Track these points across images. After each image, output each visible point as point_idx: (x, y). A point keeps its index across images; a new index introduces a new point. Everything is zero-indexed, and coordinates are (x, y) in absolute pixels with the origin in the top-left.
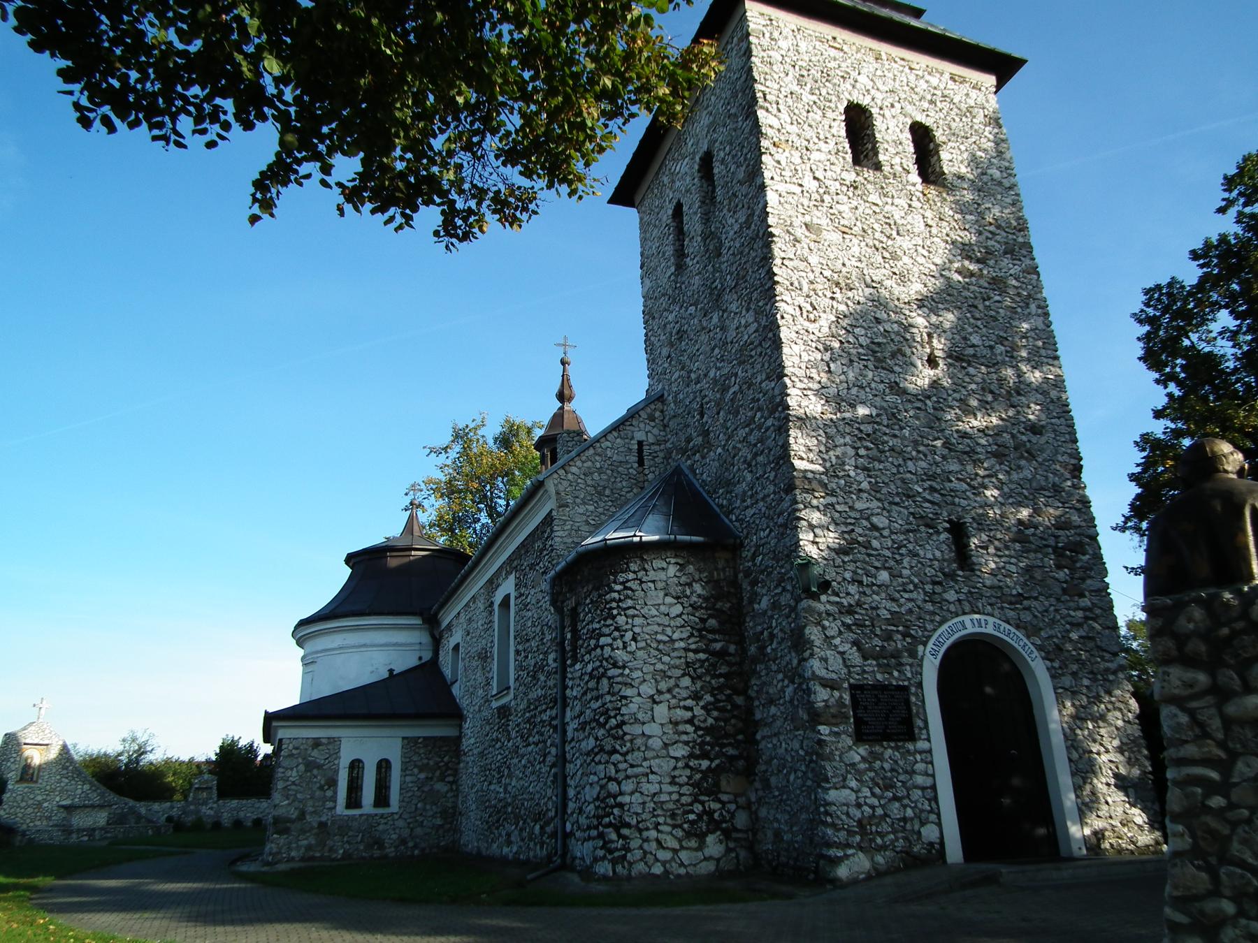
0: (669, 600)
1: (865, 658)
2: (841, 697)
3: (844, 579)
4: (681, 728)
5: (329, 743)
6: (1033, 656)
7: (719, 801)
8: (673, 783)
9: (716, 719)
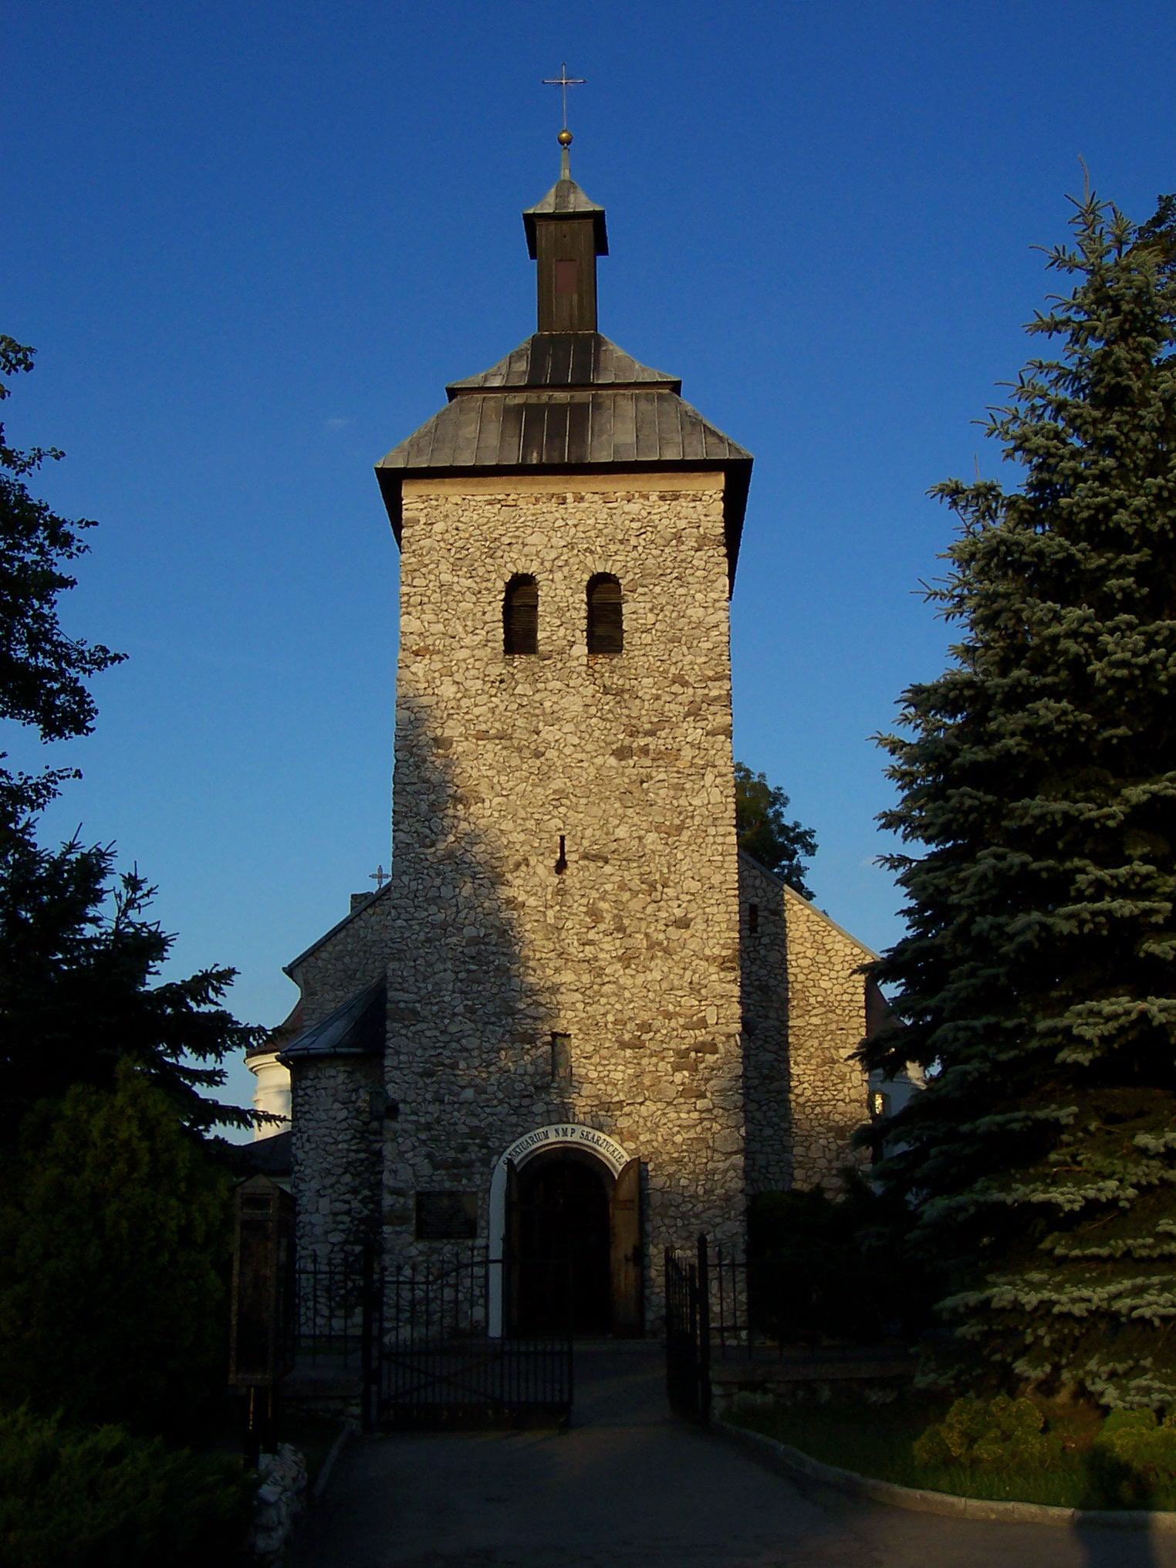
0: (337, 1105)
1: (436, 1167)
2: (405, 1203)
3: (425, 1100)
4: (339, 1218)
9: (371, 1211)
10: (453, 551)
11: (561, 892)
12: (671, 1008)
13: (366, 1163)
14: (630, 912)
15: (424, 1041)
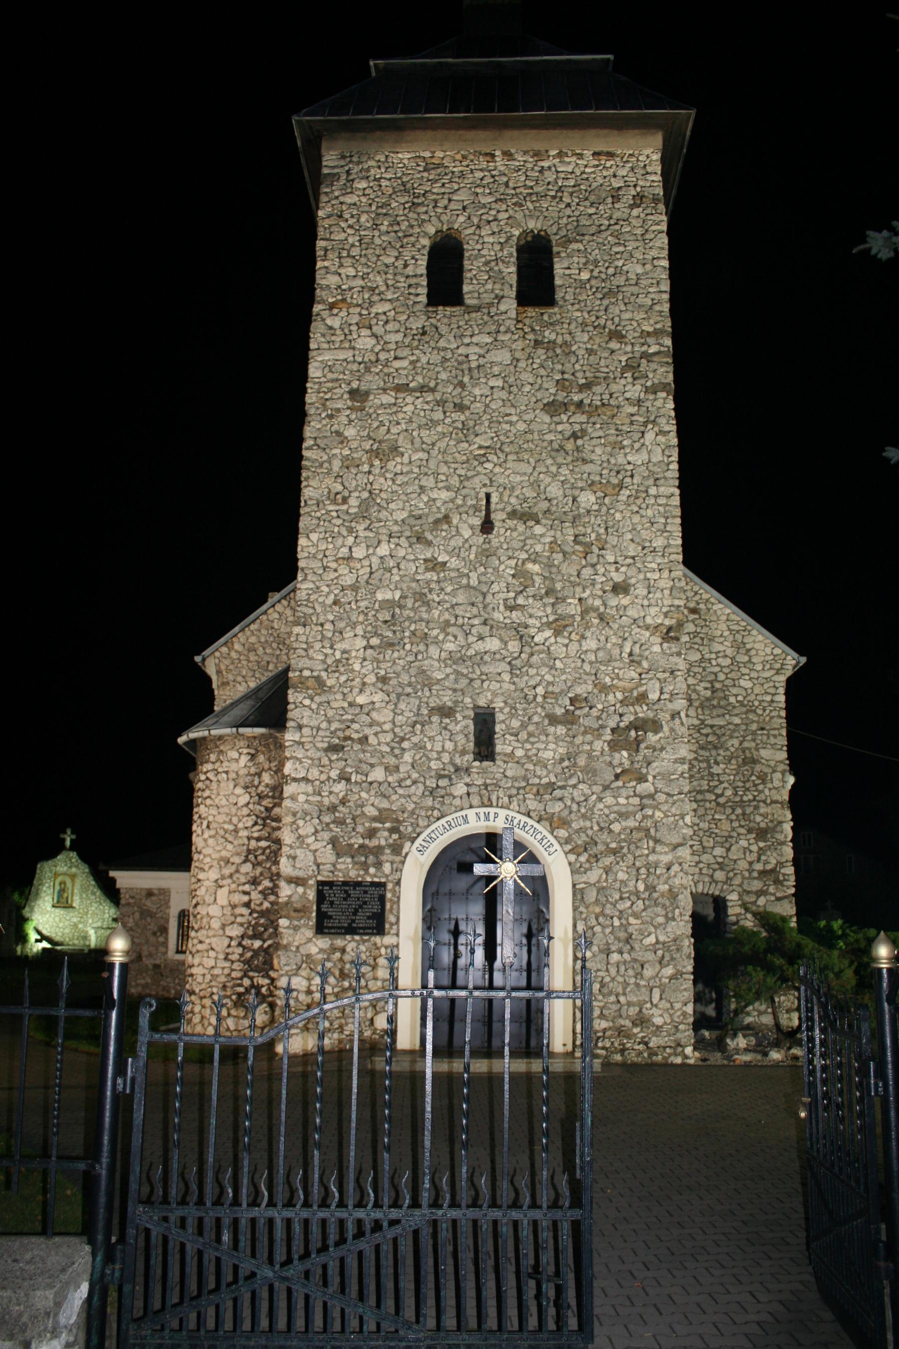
2: (305, 893)
3: (329, 778)
5: (160, 894)
6: (552, 850)
7: (269, 977)
8: (226, 959)
10: (374, 208)
11: (487, 554)
12: (608, 680)
13: (268, 851)
14: (563, 575)
15: (330, 713)
